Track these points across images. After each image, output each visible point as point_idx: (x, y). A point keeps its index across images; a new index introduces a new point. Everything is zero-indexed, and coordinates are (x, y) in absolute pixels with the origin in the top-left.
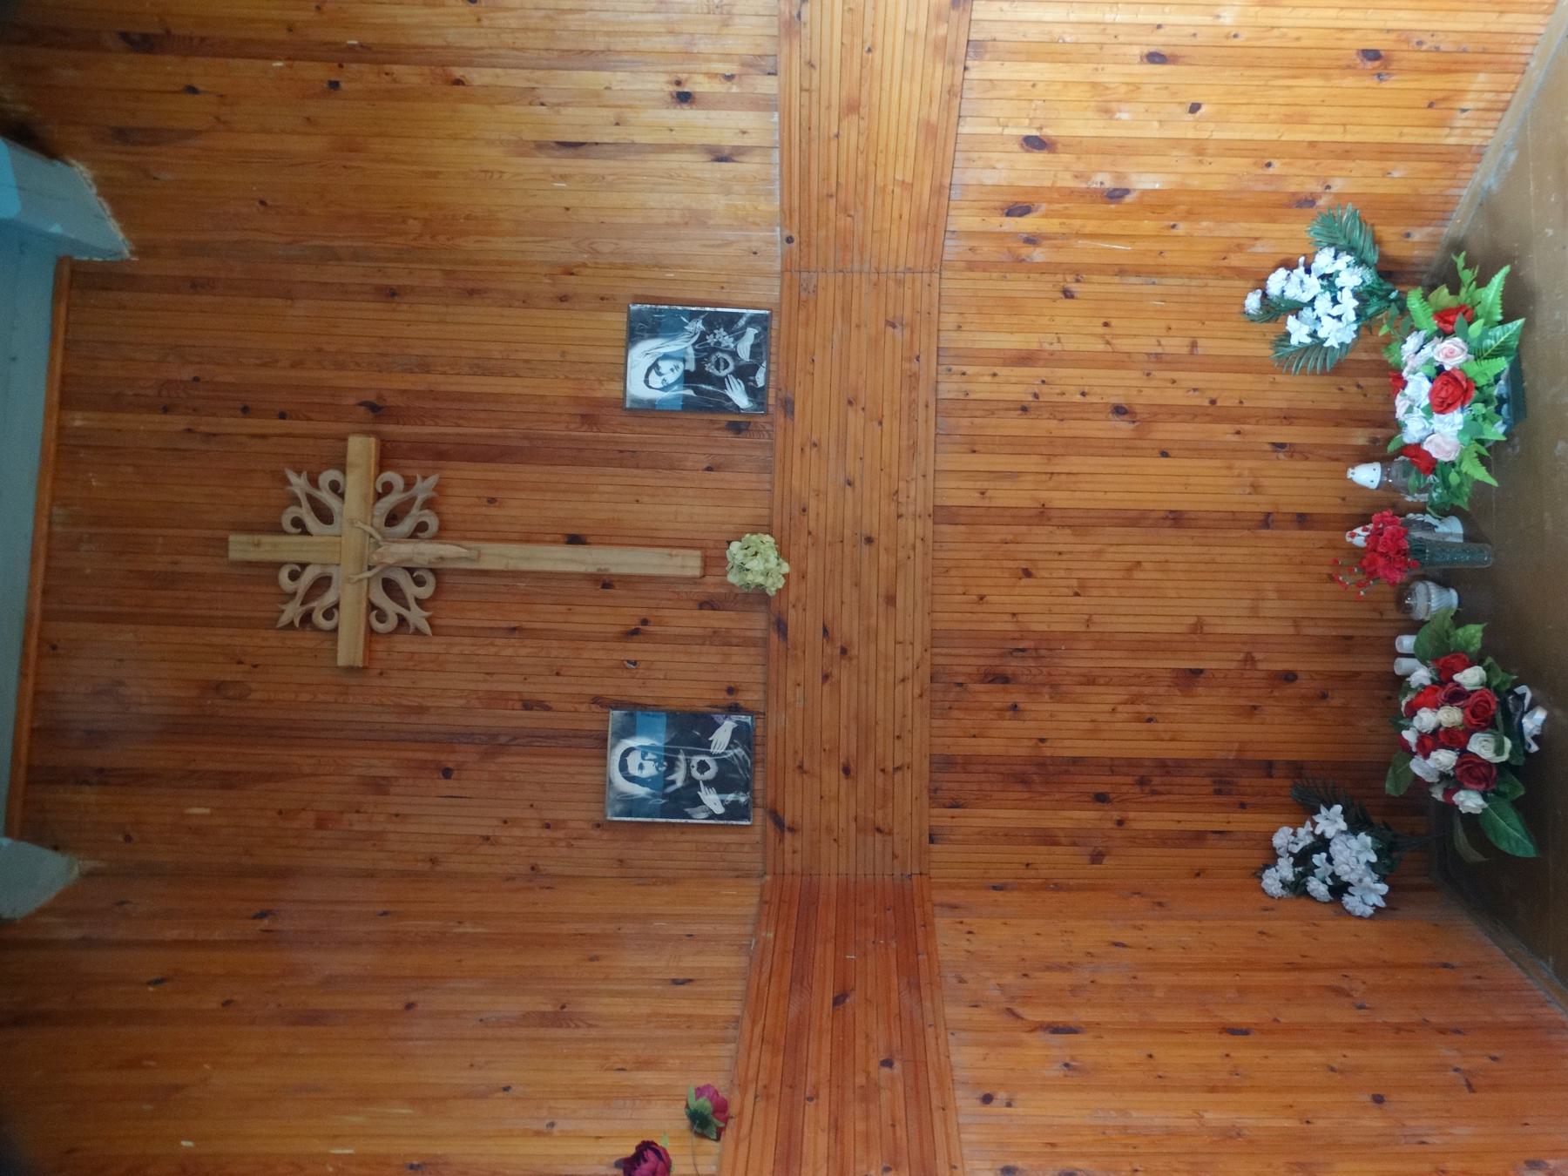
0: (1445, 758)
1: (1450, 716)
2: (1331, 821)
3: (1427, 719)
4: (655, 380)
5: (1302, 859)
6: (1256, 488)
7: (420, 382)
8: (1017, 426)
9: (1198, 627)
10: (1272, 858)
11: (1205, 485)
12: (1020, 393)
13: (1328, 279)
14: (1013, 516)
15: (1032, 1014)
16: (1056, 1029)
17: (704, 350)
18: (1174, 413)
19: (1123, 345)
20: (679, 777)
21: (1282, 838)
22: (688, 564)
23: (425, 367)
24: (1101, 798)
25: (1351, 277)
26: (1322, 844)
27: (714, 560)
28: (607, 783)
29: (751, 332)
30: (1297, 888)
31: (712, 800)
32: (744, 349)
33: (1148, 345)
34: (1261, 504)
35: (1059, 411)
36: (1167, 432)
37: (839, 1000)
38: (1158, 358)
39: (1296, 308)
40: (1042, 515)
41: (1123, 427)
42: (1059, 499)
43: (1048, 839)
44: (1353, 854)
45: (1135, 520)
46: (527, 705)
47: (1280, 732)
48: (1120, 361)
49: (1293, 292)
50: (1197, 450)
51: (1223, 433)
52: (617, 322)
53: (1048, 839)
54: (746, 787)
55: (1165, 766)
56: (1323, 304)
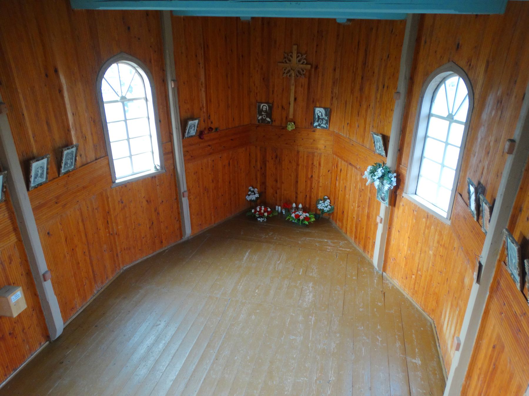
0: (258, 209)
1: (262, 211)
2: (257, 195)
3: (263, 209)
4: (318, 112)
5: (253, 192)
6: (301, 192)
7: (320, 75)
8: (310, 163)
9: (283, 183)
10: (253, 188)
11: (301, 186)
12: (315, 163)
13: (326, 207)
14: (298, 161)
15: (231, 161)
16: (229, 164)
17: (322, 119)
18: (311, 184)
19: (321, 178)
20: (263, 113)
21: (256, 189)
22: (291, 117)
23: (323, 75)
24: (261, 168)
25: (326, 209)
26: (255, 194)
27: (291, 121)
28: (262, 103)
29: (325, 126)
30: (250, 190)
31: (260, 118)
32: (322, 125)
33: (321, 181)
34: (299, 193)
35: (312, 168)
36: (309, 182)
37: (232, 140)
38: (319, 182)
39: (324, 202)
40: (298, 165)
41: (310, 176)
42: (300, 167)
43: (256, 161)
44: (253, 197)
45: (297, 177)
46: (273, 91)
47: (270, 191)
48: (319, 177)
49: (326, 202)
50: (306, 185)
51: (308, 189)
52: (328, 106)
53: (256, 161)
54: (262, 122)
55: (265, 176)
56: (324, 205)
